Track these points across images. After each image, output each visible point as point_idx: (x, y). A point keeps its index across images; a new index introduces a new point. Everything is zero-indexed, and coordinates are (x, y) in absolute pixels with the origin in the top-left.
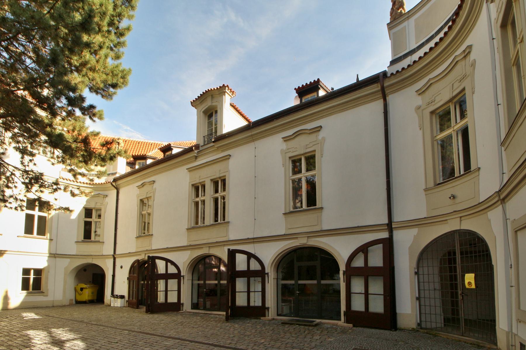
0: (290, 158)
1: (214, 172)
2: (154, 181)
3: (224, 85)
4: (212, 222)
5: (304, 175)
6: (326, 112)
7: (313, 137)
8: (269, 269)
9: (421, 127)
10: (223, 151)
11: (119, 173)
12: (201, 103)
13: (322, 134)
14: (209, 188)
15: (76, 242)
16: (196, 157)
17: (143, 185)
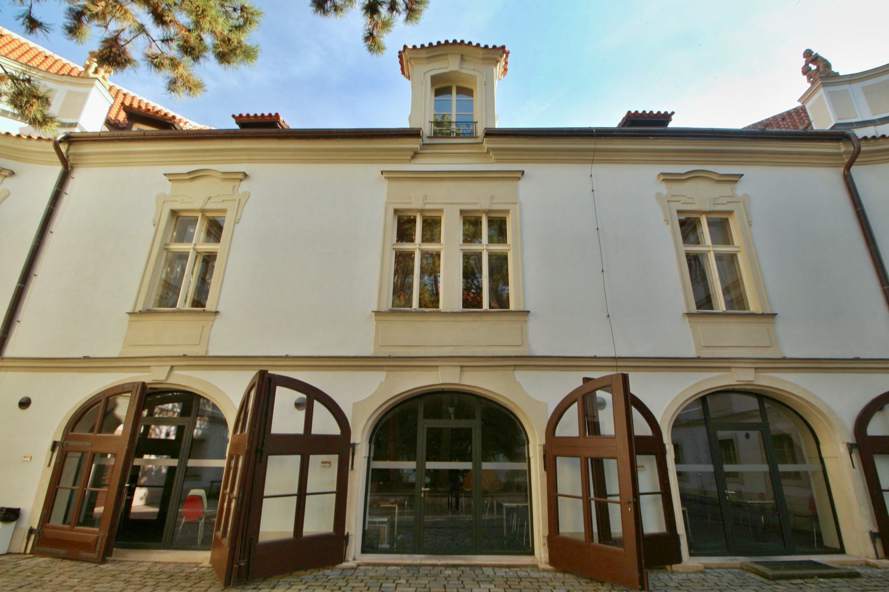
0: (679, 212)
1: (482, 197)
2: (245, 175)
3: (405, 47)
4: (458, 306)
5: (417, 246)
6: (687, 156)
7: (725, 190)
8: (360, 437)
9: (156, 225)
10: (498, 161)
11: (82, 127)
12: (484, 59)
13: (741, 189)
14: (452, 230)
15: (377, 313)
16: (415, 154)
17: (194, 176)
